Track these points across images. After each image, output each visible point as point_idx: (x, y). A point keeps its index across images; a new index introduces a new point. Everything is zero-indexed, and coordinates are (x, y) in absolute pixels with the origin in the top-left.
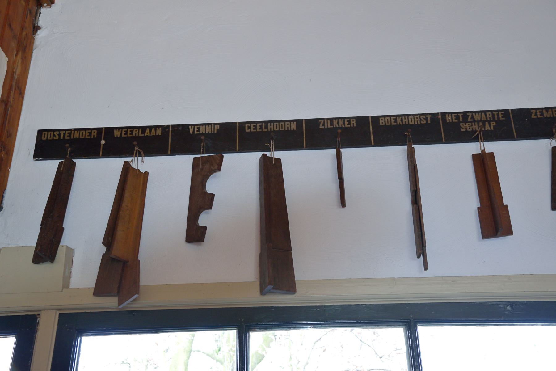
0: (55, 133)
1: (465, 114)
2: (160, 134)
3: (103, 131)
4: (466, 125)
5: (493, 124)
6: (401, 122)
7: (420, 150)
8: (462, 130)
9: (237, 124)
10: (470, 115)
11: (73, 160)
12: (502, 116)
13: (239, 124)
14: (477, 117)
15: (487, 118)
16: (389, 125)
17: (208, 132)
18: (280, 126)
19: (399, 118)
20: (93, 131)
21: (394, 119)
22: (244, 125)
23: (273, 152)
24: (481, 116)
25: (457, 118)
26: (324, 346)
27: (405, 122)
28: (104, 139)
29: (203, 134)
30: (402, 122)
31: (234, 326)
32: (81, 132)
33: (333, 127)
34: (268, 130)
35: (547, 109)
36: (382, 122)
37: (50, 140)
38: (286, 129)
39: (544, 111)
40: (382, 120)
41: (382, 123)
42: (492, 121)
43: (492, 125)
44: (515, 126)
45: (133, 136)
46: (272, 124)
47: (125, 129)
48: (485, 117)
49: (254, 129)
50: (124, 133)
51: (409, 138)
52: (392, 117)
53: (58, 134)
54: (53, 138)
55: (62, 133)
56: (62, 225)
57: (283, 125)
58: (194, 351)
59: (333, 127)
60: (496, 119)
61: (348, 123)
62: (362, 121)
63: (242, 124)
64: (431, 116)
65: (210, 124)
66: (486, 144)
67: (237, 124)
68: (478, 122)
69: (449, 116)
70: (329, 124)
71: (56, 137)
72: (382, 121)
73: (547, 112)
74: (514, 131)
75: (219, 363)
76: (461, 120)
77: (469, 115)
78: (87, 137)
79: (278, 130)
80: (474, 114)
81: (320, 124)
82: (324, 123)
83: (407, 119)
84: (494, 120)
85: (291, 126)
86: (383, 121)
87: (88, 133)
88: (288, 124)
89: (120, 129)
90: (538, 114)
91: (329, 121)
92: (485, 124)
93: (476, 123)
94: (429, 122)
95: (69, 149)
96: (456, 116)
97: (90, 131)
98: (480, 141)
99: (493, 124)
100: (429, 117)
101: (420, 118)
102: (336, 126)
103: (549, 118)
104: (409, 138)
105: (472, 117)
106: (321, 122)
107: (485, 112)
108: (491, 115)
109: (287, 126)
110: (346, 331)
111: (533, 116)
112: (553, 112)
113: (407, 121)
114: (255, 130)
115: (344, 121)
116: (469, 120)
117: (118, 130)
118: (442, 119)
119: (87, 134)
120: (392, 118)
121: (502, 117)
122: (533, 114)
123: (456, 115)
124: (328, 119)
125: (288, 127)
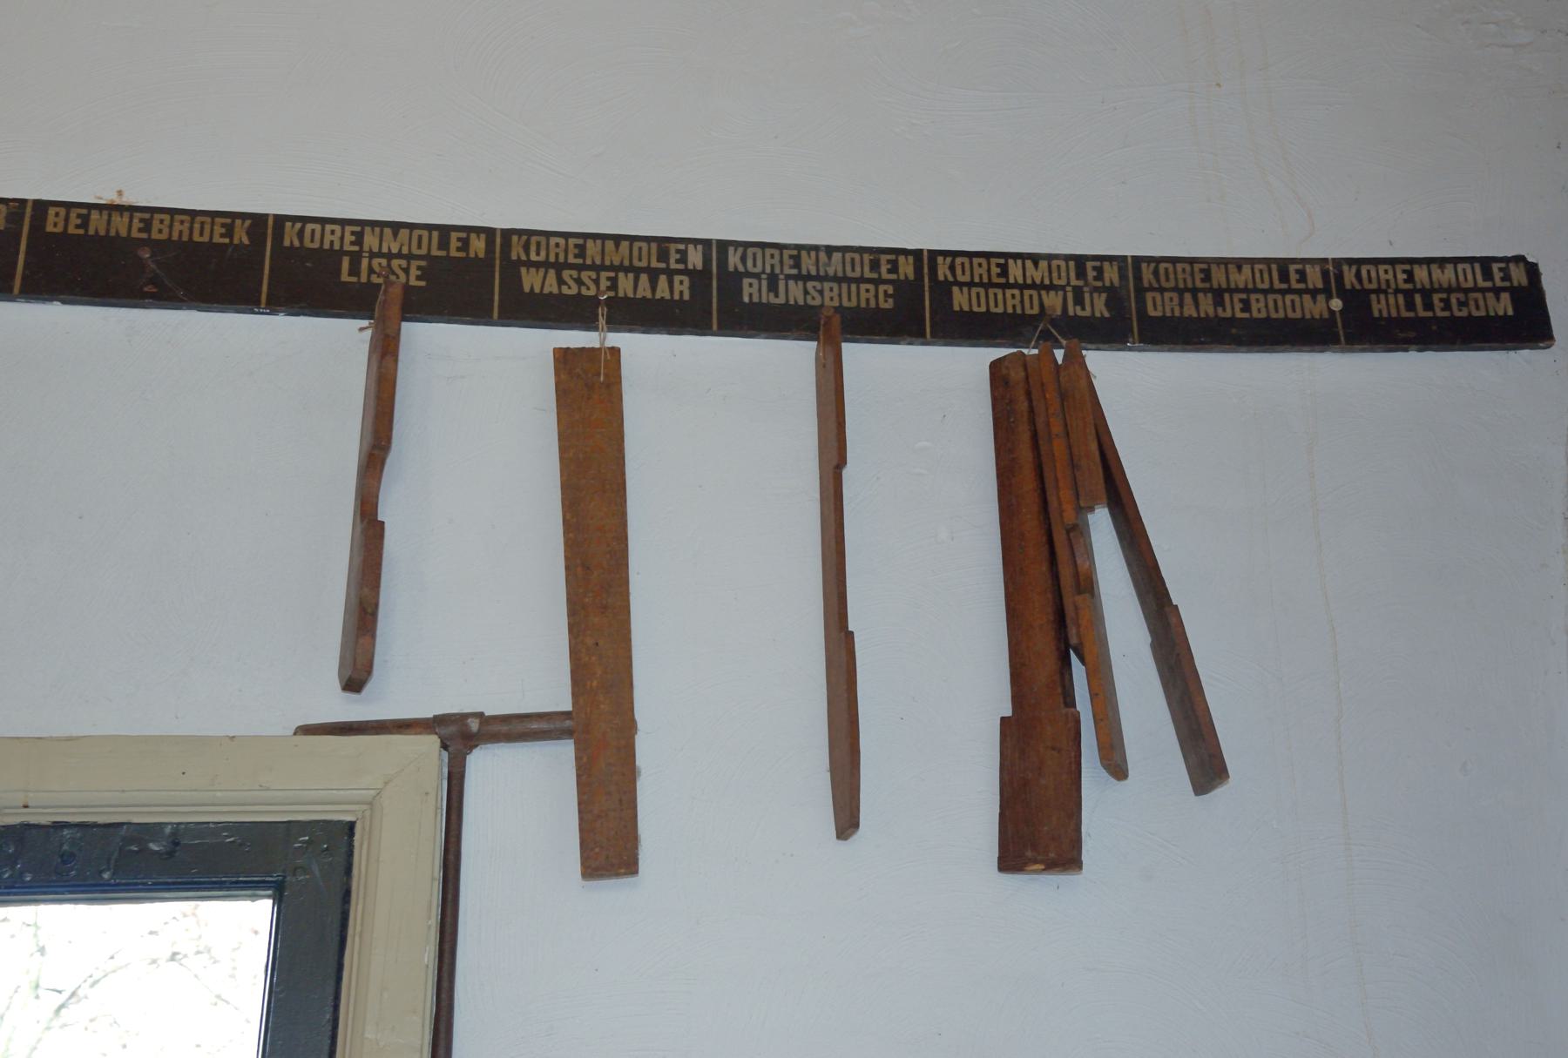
3: (29, 210)
7: (859, 357)
20: (157, 216)
21: (998, 265)
26: (91, 976)
33: (448, 256)
34: (1104, 285)
45: (86, 234)
47: (226, 217)
49: (458, 249)
57: (423, 238)
59: (448, 256)
65: (816, 248)
66: (611, 335)
75: (19, 990)
78: (217, 239)
110: (153, 930)
112: (215, 227)
114: (462, 254)
119: (218, 230)
124: (1068, 258)
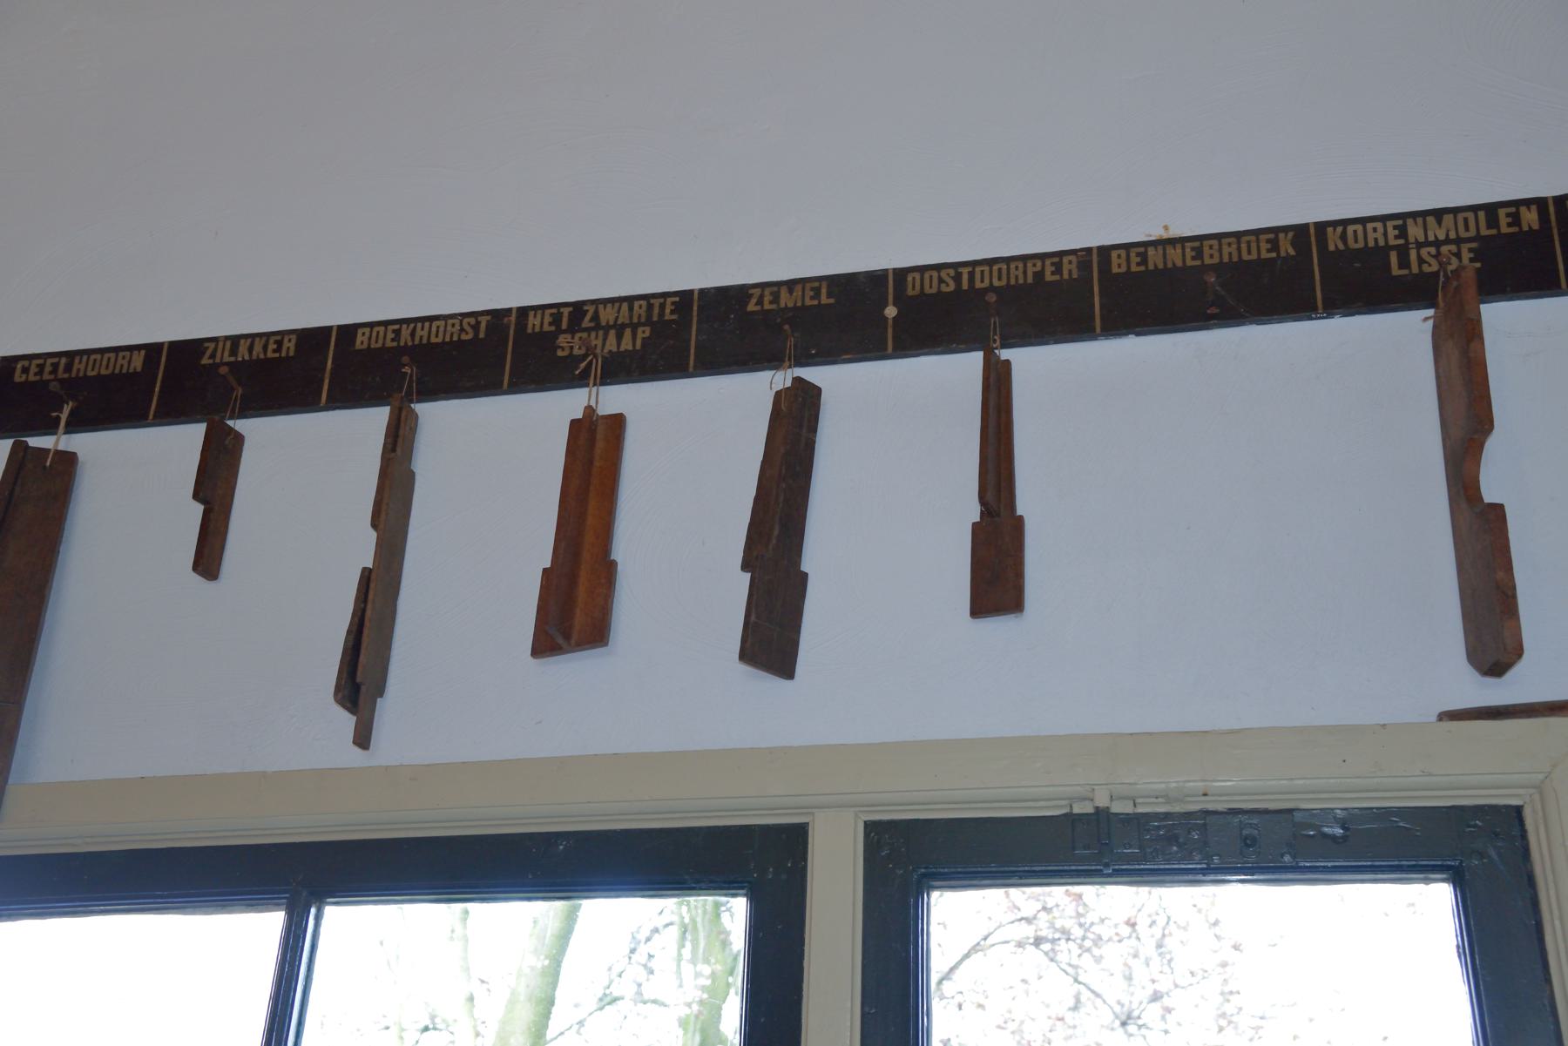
0: (943, 274)
1: (578, 308)
2: (139, 369)
4: (573, 338)
5: (644, 332)
6: (409, 338)
8: (560, 353)
9: (1312, 230)
10: (591, 309)
11: (230, 423)
12: (671, 310)
13: (1099, 255)
14: (607, 315)
15: (631, 317)
16: (379, 348)
17: (1436, 236)
18: (995, 274)
19: (1335, 230)
20: (1206, 243)
22: (13, 365)
23: (595, 389)
24: (619, 312)
25: (556, 320)
27: (1376, 240)
28: (894, 305)
29: (1212, 267)
30: (413, 340)
31: (736, 885)
32: (927, 276)
34: (819, 302)
35: (791, 284)
36: (1334, 242)
37: (375, 349)
38: (1226, 259)
39: (1431, 220)
40: (1017, 268)
41: (362, 343)
42: (644, 325)
43: (640, 335)
44: (697, 336)
46: (85, 358)
48: (627, 314)
50: (1189, 253)
51: (410, 386)
52: (1186, 244)
53: (952, 277)
54: (939, 287)
55: (965, 271)
56: (798, 563)
58: (1070, 959)
59: (280, 357)
60: (655, 318)
61: (1139, 259)
62: (313, 339)
63: (901, 274)
64: (489, 318)
67: (1312, 230)
68: (607, 328)
69: (535, 316)
70: (226, 353)
71: (948, 285)
72: (1120, 261)
73: (791, 292)
74: (692, 351)
76: (564, 326)
77: (588, 311)
79: (988, 285)
80: (601, 307)
81: (204, 353)
82: (215, 349)
83: (1261, 249)
84: (649, 322)
85: (129, 362)
86: (1123, 261)
87: (1193, 249)
88: (1017, 268)
89: (412, 322)
90: (766, 299)
91: (1481, 214)
92: (623, 333)
93: (601, 333)
94: (482, 335)
95: (68, 404)
96: (554, 314)
97: (1056, 260)
98: (591, 384)
99: (644, 332)
100: (484, 320)
101: (461, 324)
102: (243, 358)
103: (791, 309)
104: (410, 386)
105: (596, 317)
106: (208, 348)
107: (630, 300)
108: (644, 308)
109: (1371, 236)
111: (751, 307)
113: (806, 292)
115: (267, 342)
116: (584, 325)
117: (609, 305)
118: (516, 325)
120: (1390, 224)
121: (672, 312)
122: (754, 301)
123: (554, 311)
125: (1017, 277)
